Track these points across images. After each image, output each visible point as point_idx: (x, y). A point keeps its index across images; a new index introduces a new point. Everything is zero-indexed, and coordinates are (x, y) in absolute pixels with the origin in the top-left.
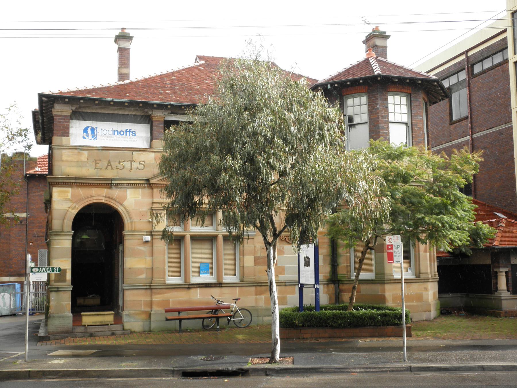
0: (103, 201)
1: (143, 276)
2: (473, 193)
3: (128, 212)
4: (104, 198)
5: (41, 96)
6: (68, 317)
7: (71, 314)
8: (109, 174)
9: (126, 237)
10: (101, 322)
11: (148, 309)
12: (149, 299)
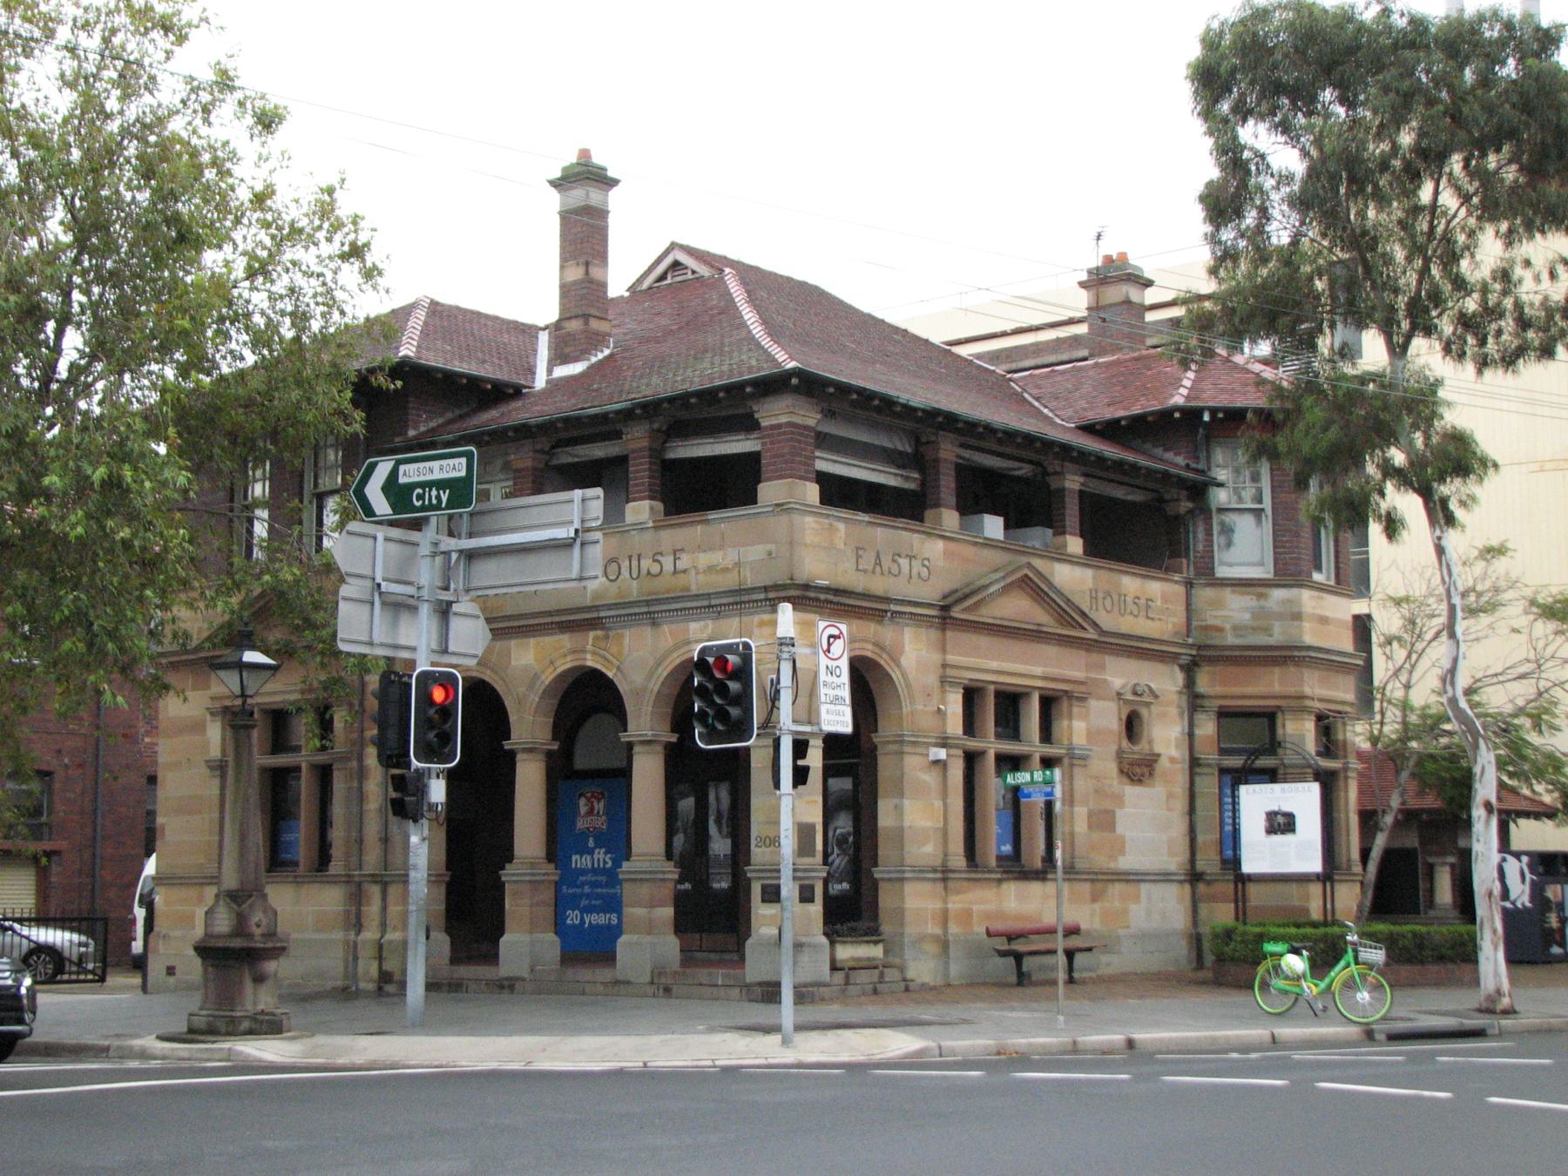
0: (869, 654)
1: (929, 848)
2: (1175, 461)
3: (908, 685)
4: (870, 647)
5: (1202, 199)
6: (821, 946)
7: (824, 940)
8: (878, 585)
9: (880, 751)
10: (869, 959)
11: (938, 931)
12: (939, 905)
